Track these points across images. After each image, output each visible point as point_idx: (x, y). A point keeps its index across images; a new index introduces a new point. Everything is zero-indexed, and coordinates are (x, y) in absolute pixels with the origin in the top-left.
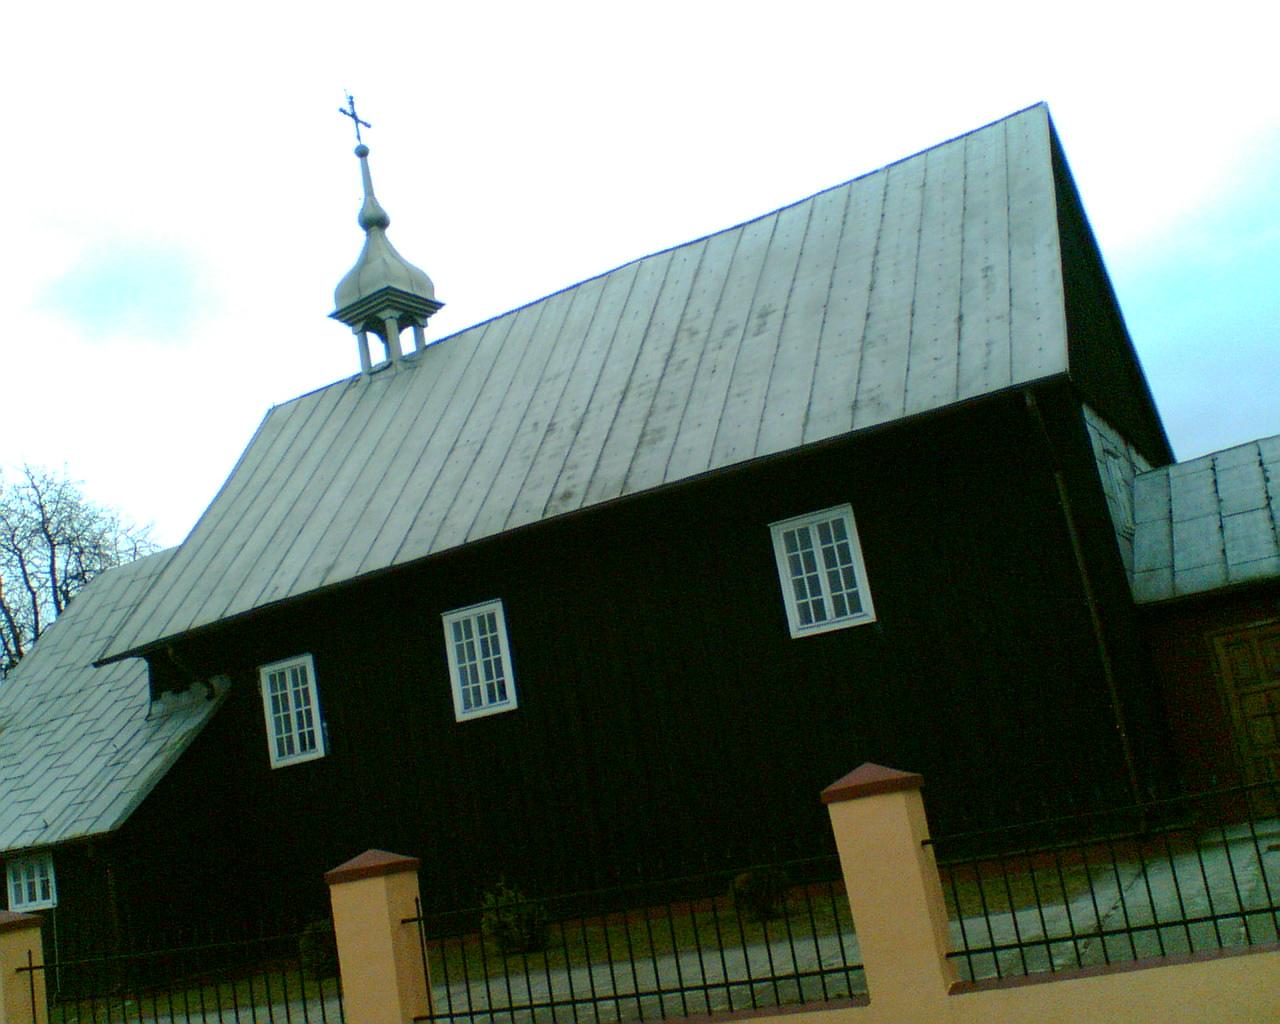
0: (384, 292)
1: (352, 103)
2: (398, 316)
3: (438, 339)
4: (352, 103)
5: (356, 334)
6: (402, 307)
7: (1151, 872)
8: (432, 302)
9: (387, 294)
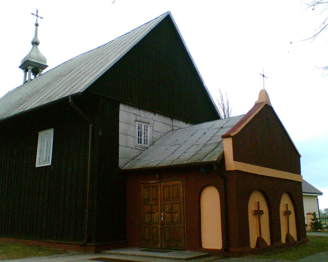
0: (27, 62)
1: (37, 12)
2: (32, 68)
3: (212, 97)
4: (37, 12)
5: (24, 72)
6: (33, 66)
7: (173, 120)
8: (46, 65)
9: (28, 62)
